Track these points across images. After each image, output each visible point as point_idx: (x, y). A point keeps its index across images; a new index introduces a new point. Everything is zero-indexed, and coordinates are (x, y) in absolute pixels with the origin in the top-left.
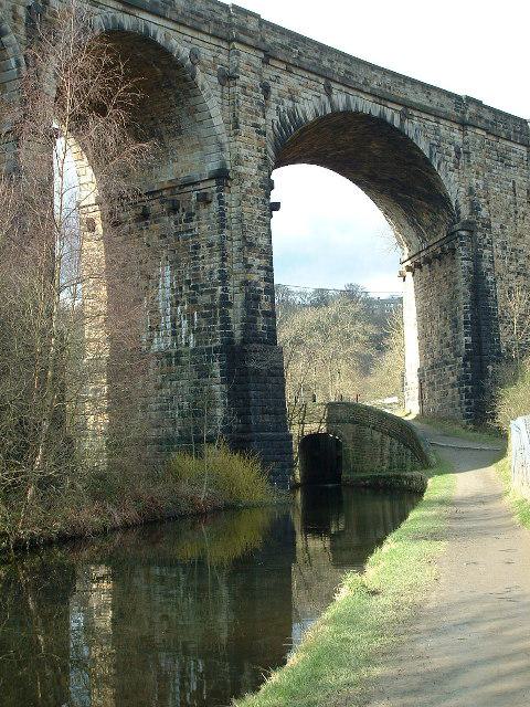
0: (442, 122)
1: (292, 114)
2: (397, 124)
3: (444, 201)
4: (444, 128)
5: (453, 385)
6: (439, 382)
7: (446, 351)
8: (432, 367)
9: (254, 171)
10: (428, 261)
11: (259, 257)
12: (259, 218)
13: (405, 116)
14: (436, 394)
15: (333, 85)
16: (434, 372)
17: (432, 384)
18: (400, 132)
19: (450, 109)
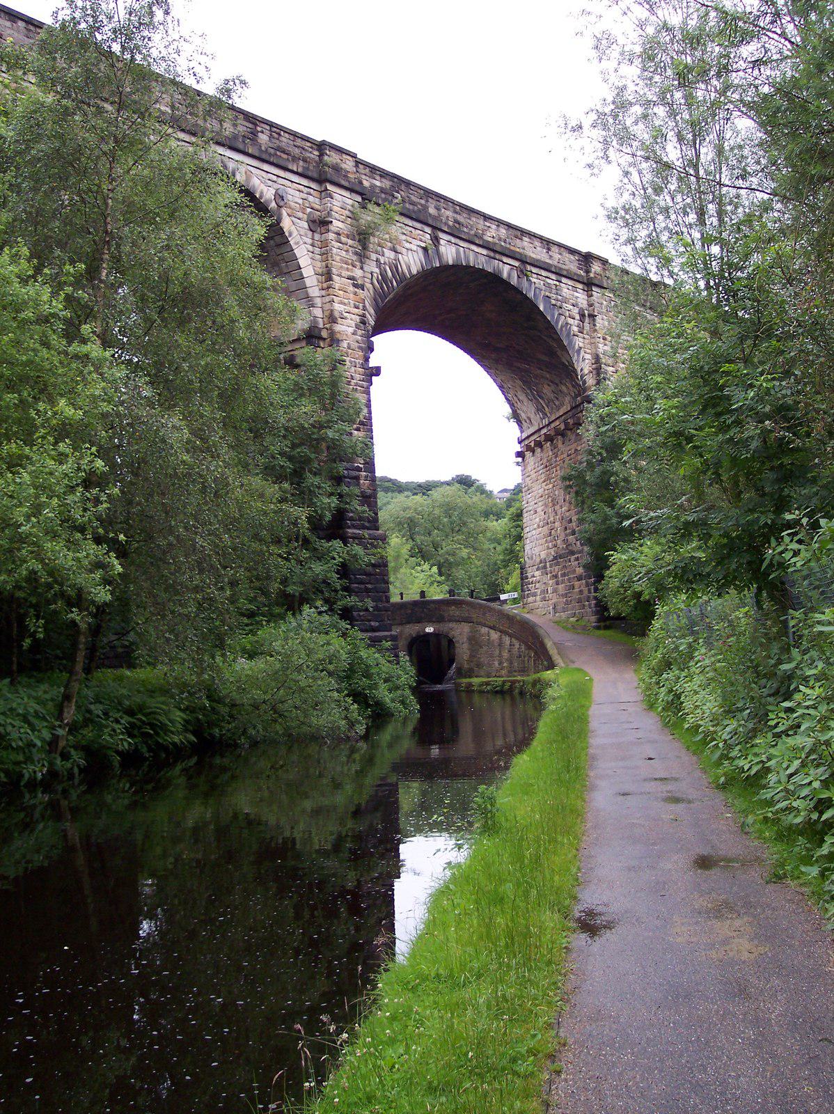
0: (564, 280)
1: (395, 267)
2: (514, 281)
3: (568, 372)
4: (566, 288)
5: (579, 578)
6: (564, 575)
8: (555, 558)
9: (351, 330)
10: (549, 438)
11: (358, 429)
12: (356, 385)
13: (523, 273)
15: (441, 235)
16: (558, 564)
17: (556, 576)
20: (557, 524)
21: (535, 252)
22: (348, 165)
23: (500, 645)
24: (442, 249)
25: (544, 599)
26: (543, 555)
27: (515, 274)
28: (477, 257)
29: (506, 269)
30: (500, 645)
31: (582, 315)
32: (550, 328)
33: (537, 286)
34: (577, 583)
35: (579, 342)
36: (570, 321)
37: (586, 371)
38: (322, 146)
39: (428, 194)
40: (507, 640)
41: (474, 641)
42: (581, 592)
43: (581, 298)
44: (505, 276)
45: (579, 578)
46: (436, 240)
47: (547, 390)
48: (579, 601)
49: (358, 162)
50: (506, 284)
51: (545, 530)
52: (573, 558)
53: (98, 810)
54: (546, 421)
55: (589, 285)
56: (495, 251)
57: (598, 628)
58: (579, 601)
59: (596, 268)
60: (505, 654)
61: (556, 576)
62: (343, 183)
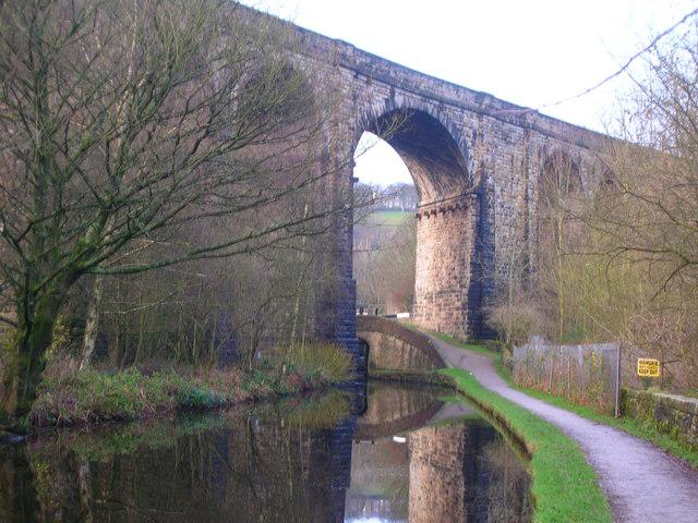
1: (369, 114)
2: (435, 115)
3: (462, 171)
5: (457, 309)
7: (453, 282)
14: (443, 314)
17: (440, 305)
18: (437, 120)
19: (472, 103)
20: (443, 270)
21: (450, 95)
22: (349, 52)
23: (403, 350)
24: (396, 98)
25: (429, 319)
26: (430, 289)
27: (436, 111)
28: (414, 102)
29: (430, 108)
30: (403, 350)
31: (475, 135)
32: (454, 144)
33: (448, 117)
34: (455, 313)
35: (471, 152)
36: (467, 139)
37: (474, 172)
38: (336, 42)
39: (390, 64)
40: (408, 347)
41: (384, 345)
42: (457, 318)
43: (475, 122)
44: (430, 112)
45: (457, 309)
46: (393, 93)
47: (444, 179)
48: (456, 324)
49: (355, 49)
50: (430, 117)
51: (434, 272)
52: (453, 295)
53: (227, 89)
54: (441, 198)
55: (481, 114)
56: (426, 97)
57: (469, 343)
58: (456, 324)
59: (487, 101)
60: (406, 356)
61: (440, 305)
62: (347, 65)
